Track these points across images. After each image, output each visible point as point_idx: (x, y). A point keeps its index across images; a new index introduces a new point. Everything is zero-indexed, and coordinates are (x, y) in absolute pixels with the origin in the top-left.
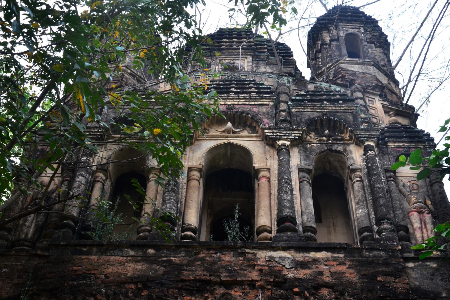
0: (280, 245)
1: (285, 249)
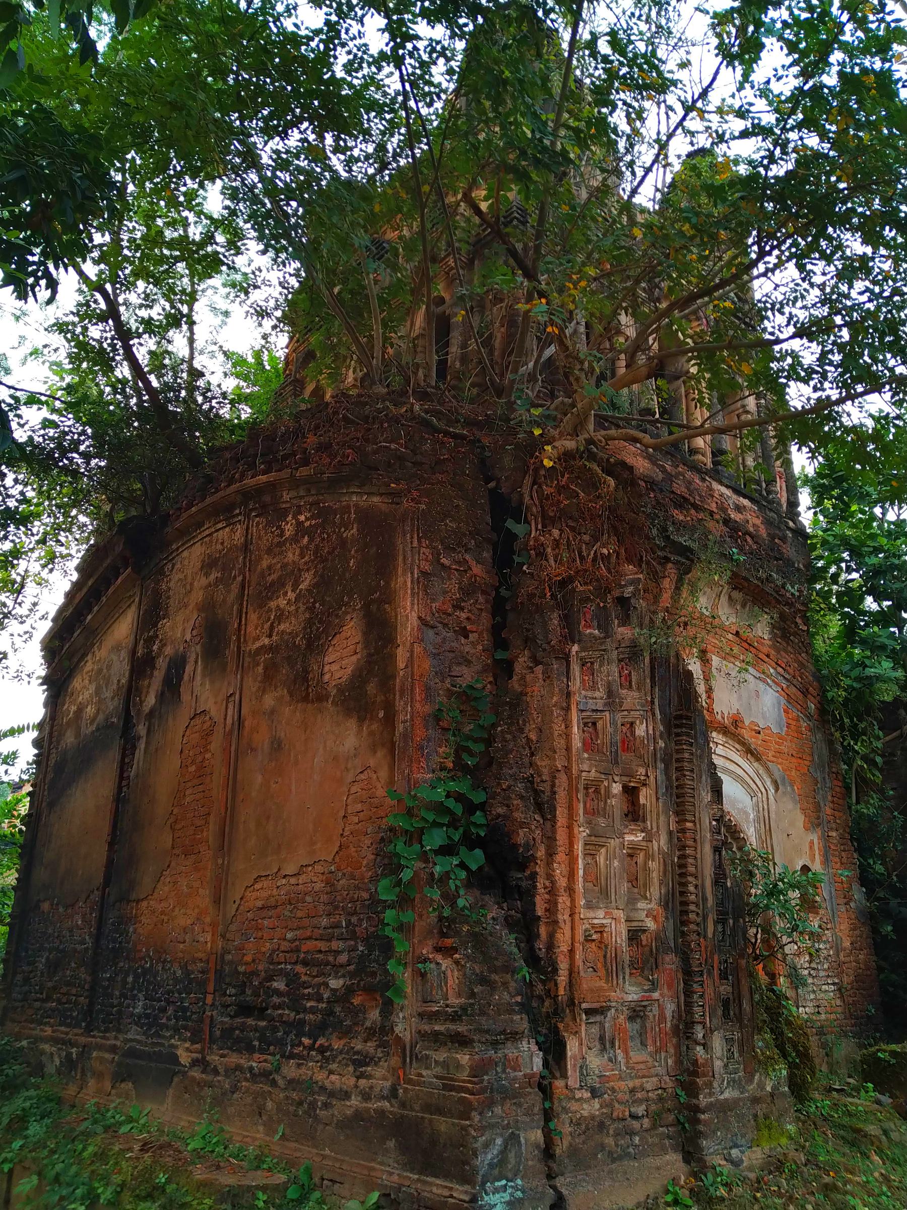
0: (725, 481)
1: (727, 487)
